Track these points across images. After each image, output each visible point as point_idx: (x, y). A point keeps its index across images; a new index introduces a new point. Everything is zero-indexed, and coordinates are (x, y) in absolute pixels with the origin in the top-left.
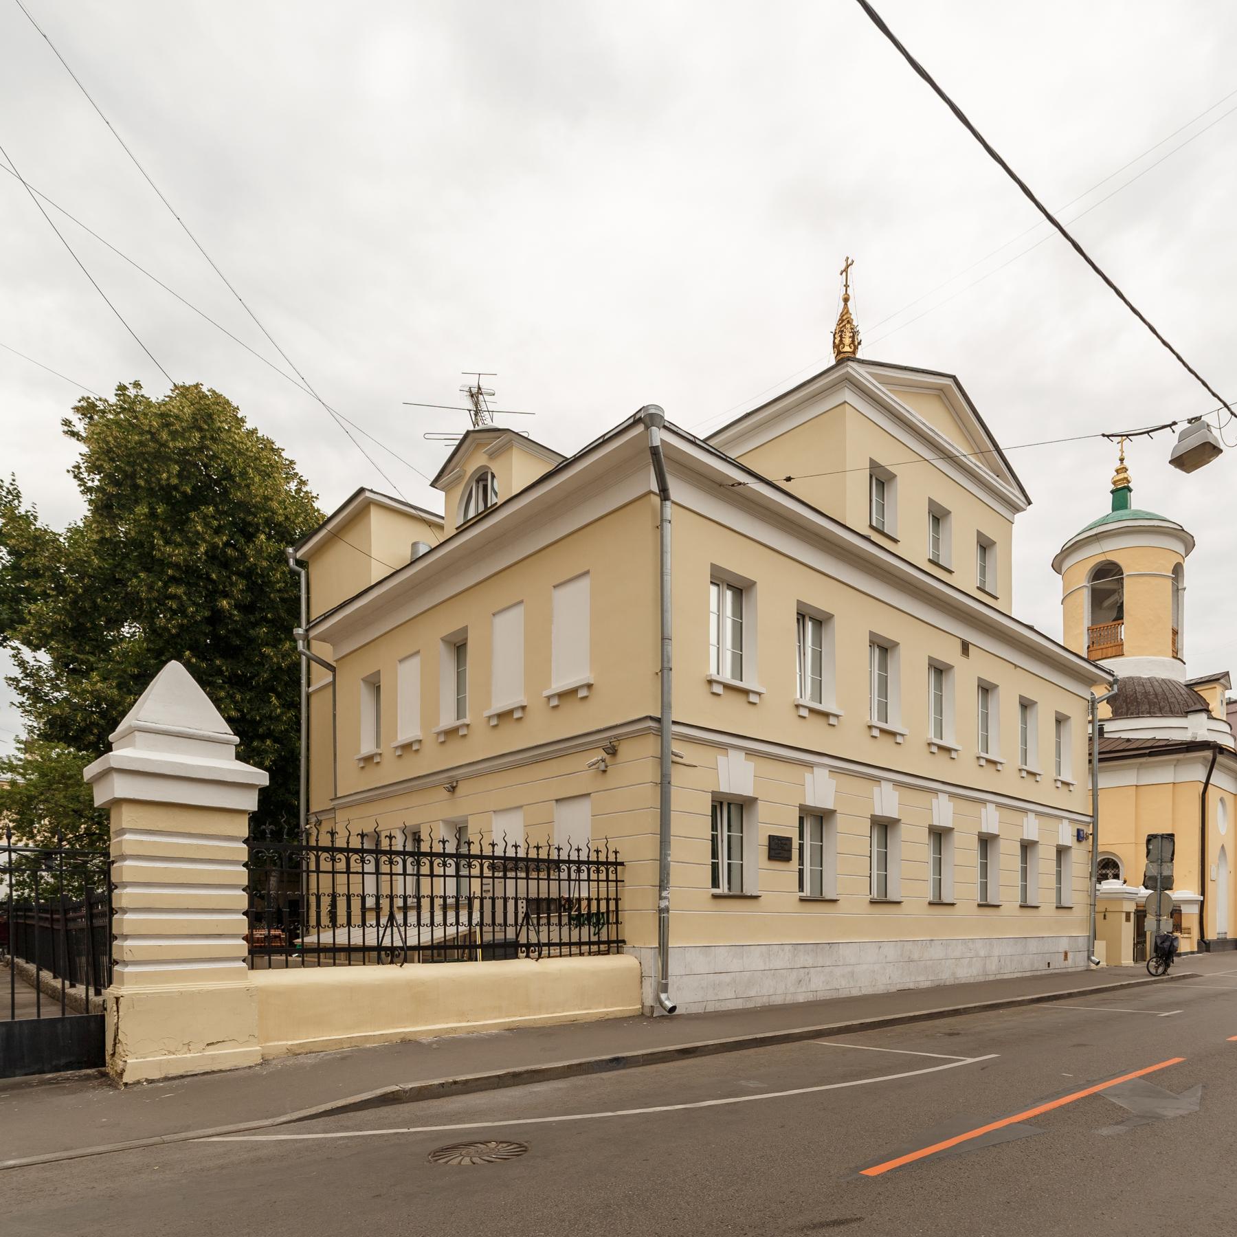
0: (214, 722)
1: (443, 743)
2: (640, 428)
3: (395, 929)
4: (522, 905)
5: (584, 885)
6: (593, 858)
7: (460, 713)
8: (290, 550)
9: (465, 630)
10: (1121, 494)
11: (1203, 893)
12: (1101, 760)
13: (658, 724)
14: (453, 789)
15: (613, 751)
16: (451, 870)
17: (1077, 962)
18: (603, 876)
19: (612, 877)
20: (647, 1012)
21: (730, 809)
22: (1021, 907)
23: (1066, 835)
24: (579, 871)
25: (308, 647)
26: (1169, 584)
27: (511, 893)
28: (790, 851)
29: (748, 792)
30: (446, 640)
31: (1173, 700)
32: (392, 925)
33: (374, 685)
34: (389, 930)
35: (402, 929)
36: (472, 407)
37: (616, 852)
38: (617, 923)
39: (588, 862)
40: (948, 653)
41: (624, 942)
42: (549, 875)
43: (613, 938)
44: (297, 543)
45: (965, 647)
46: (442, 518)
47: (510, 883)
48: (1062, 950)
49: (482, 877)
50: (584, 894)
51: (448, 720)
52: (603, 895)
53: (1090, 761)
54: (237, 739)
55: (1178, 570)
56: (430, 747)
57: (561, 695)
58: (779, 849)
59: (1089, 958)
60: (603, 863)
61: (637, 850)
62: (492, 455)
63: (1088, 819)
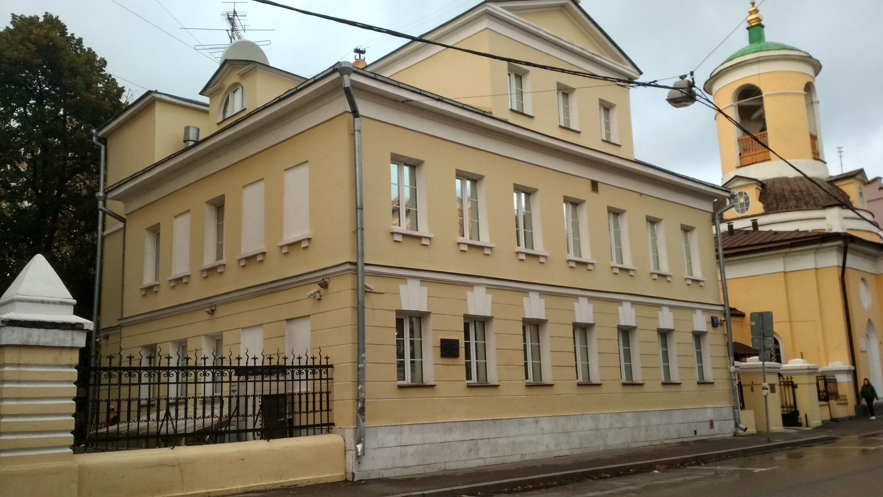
0: (62, 292)
1: (205, 277)
2: (336, 75)
3: (169, 422)
4: (258, 401)
5: (304, 383)
6: (310, 363)
7: (219, 256)
8: (94, 131)
9: (223, 196)
10: (756, 29)
11: (854, 363)
12: (726, 256)
13: (354, 267)
14: (212, 312)
15: (324, 285)
16: (209, 379)
17: (725, 429)
18: (317, 376)
19: (324, 376)
20: (350, 478)
21: (410, 322)
22: (699, 383)
23: (700, 322)
24: (314, 373)
25: (104, 205)
26: (802, 100)
27: (250, 392)
28: (457, 350)
29: (423, 308)
30: (211, 203)
31: (817, 195)
32: (167, 419)
33: (155, 230)
34: (165, 422)
35: (174, 422)
36: (229, 27)
37: (327, 358)
38: (328, 410)
39: (307, 367)
40: (582, 191)
41: (333, 424)
42: (278, 377)
43: (325, 421)
44: (99, 126)
45: (595, 185)
46: (207, 106)
47: (250, 385)
48: (709, 419)
49: (230, 381)
50: (297, 390)
51: (209, 260)
52: (317, 390)
53: (718, 257)
54: (75, 301)
55: (809, 87)
56: (196, 280)
57: (289, 245)
58: (449, 349)
59: (737, 426)
60: (317, 367)
61: (341, 356)
62: (243, 76)
63: (721, 308)
